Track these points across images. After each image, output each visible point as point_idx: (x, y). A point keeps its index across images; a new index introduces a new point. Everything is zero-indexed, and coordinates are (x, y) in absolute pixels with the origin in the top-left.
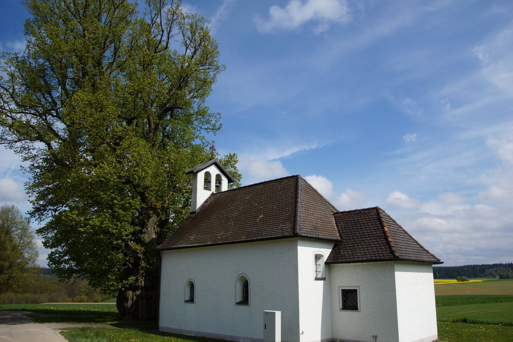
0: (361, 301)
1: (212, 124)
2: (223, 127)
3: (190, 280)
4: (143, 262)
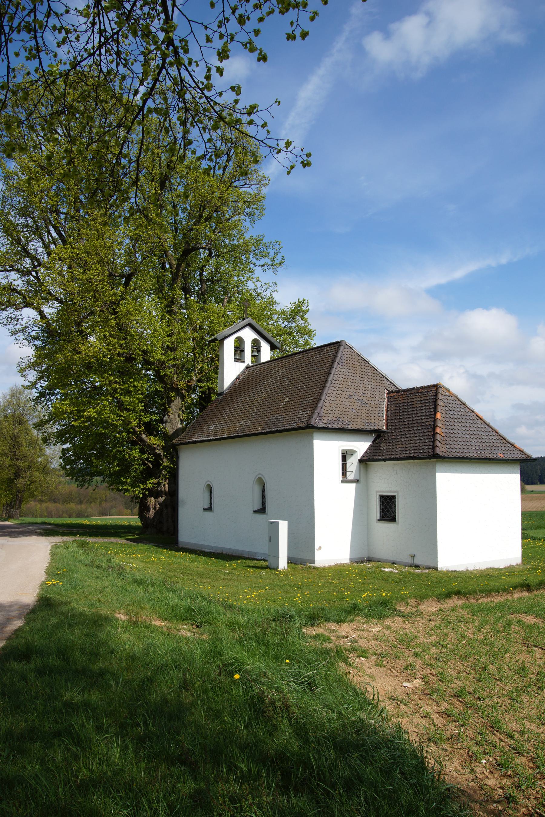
0: (399, 511)
1: (270, 257)
2: (286, 262)
3: (208, 483)
4: (165, 460)
